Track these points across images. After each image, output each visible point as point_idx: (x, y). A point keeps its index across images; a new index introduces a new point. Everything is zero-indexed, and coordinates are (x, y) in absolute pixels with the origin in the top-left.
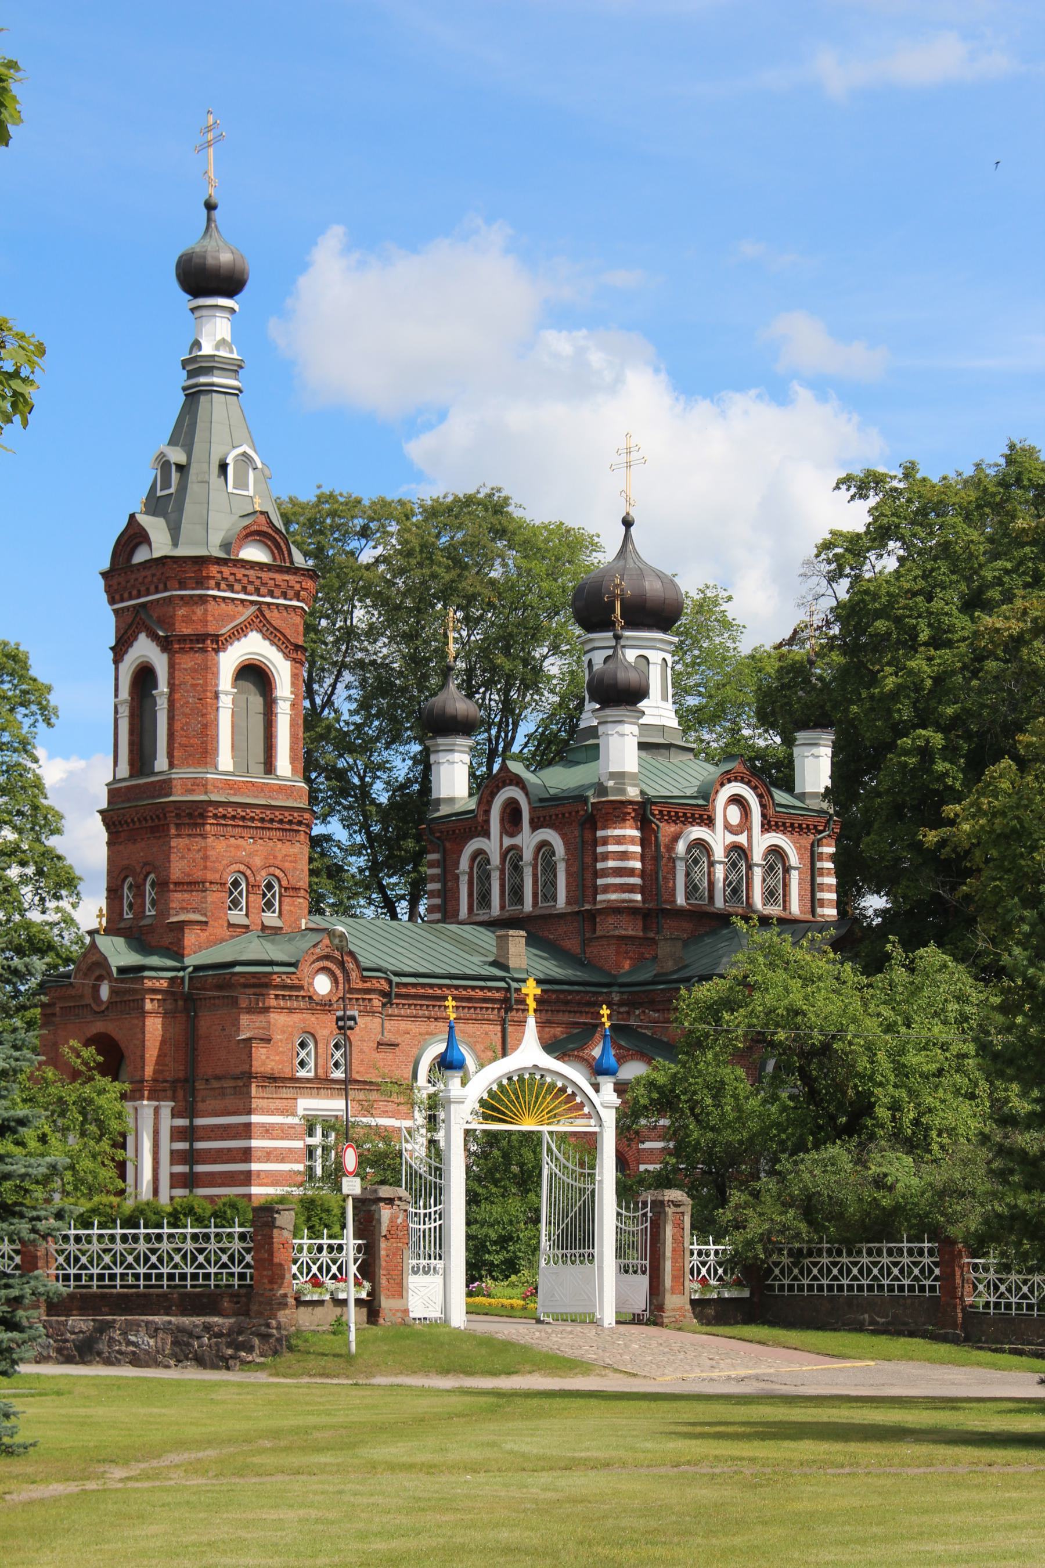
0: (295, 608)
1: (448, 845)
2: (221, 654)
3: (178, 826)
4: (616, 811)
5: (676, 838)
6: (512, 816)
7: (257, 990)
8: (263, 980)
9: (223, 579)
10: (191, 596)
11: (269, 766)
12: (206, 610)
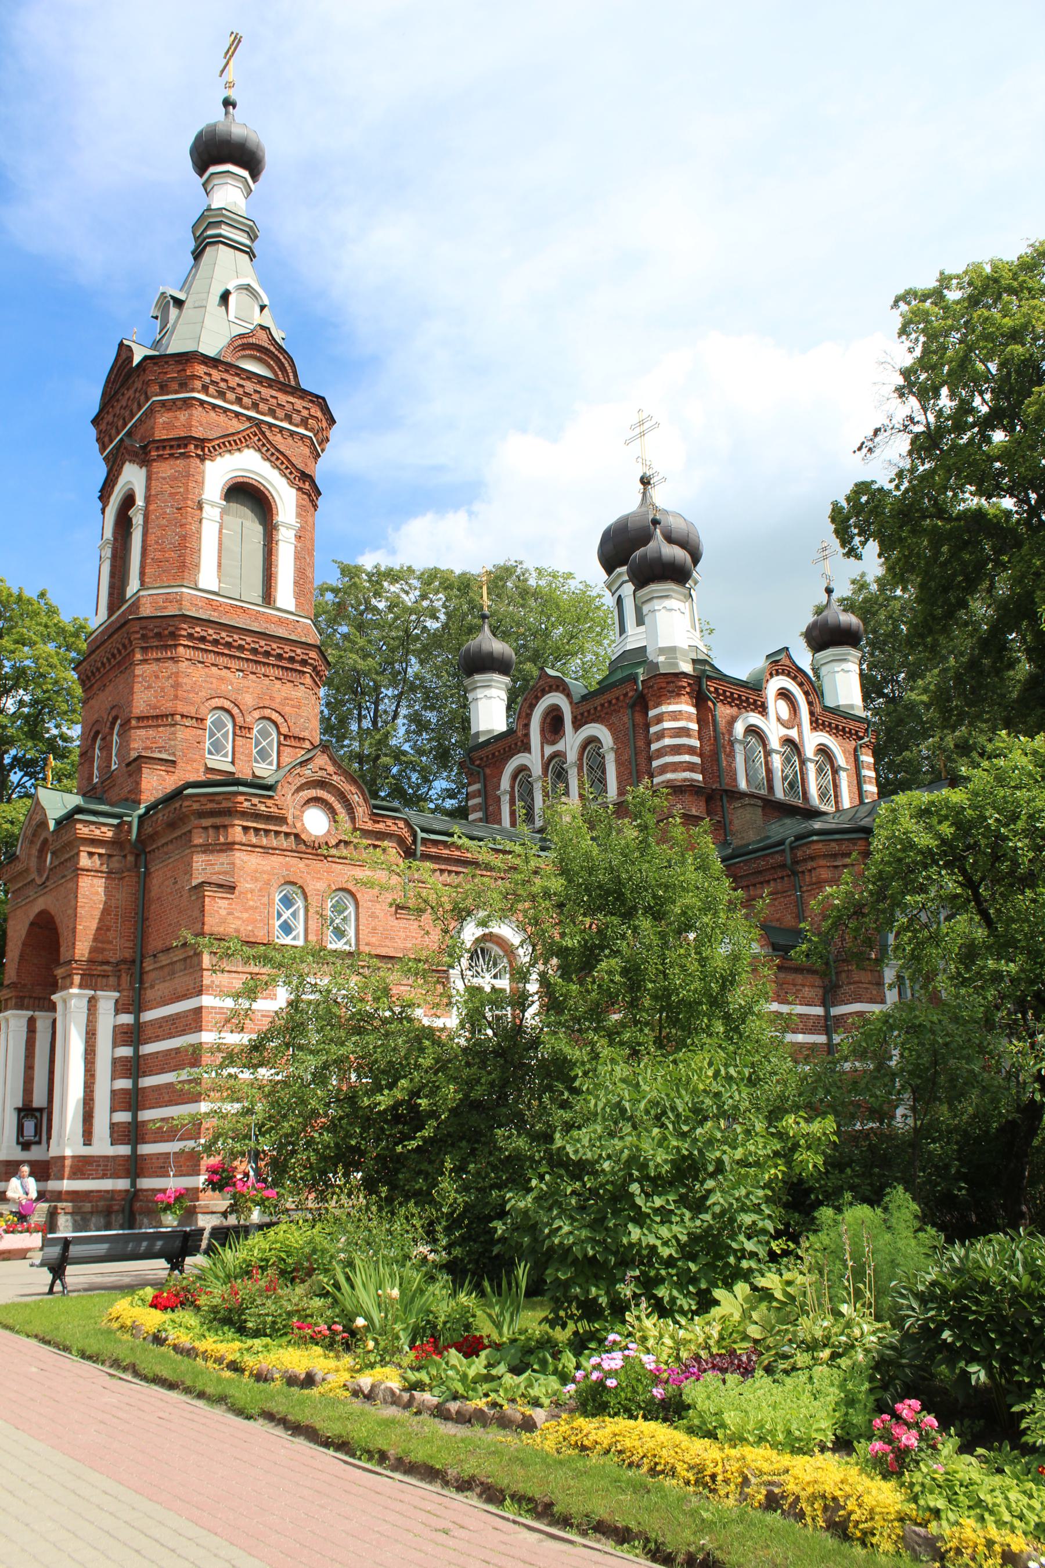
0: (303, 437)
1: (488, 771)
2: (207, 463)
3: (145, 650)
4: (668, 684)
5: (732, 721)
6: (554, 724)
7: (218, 821)
8: (226, 804)
9: (213, 382)
10: (174, 401)
11: (268, 597)
12: (191, 415)
